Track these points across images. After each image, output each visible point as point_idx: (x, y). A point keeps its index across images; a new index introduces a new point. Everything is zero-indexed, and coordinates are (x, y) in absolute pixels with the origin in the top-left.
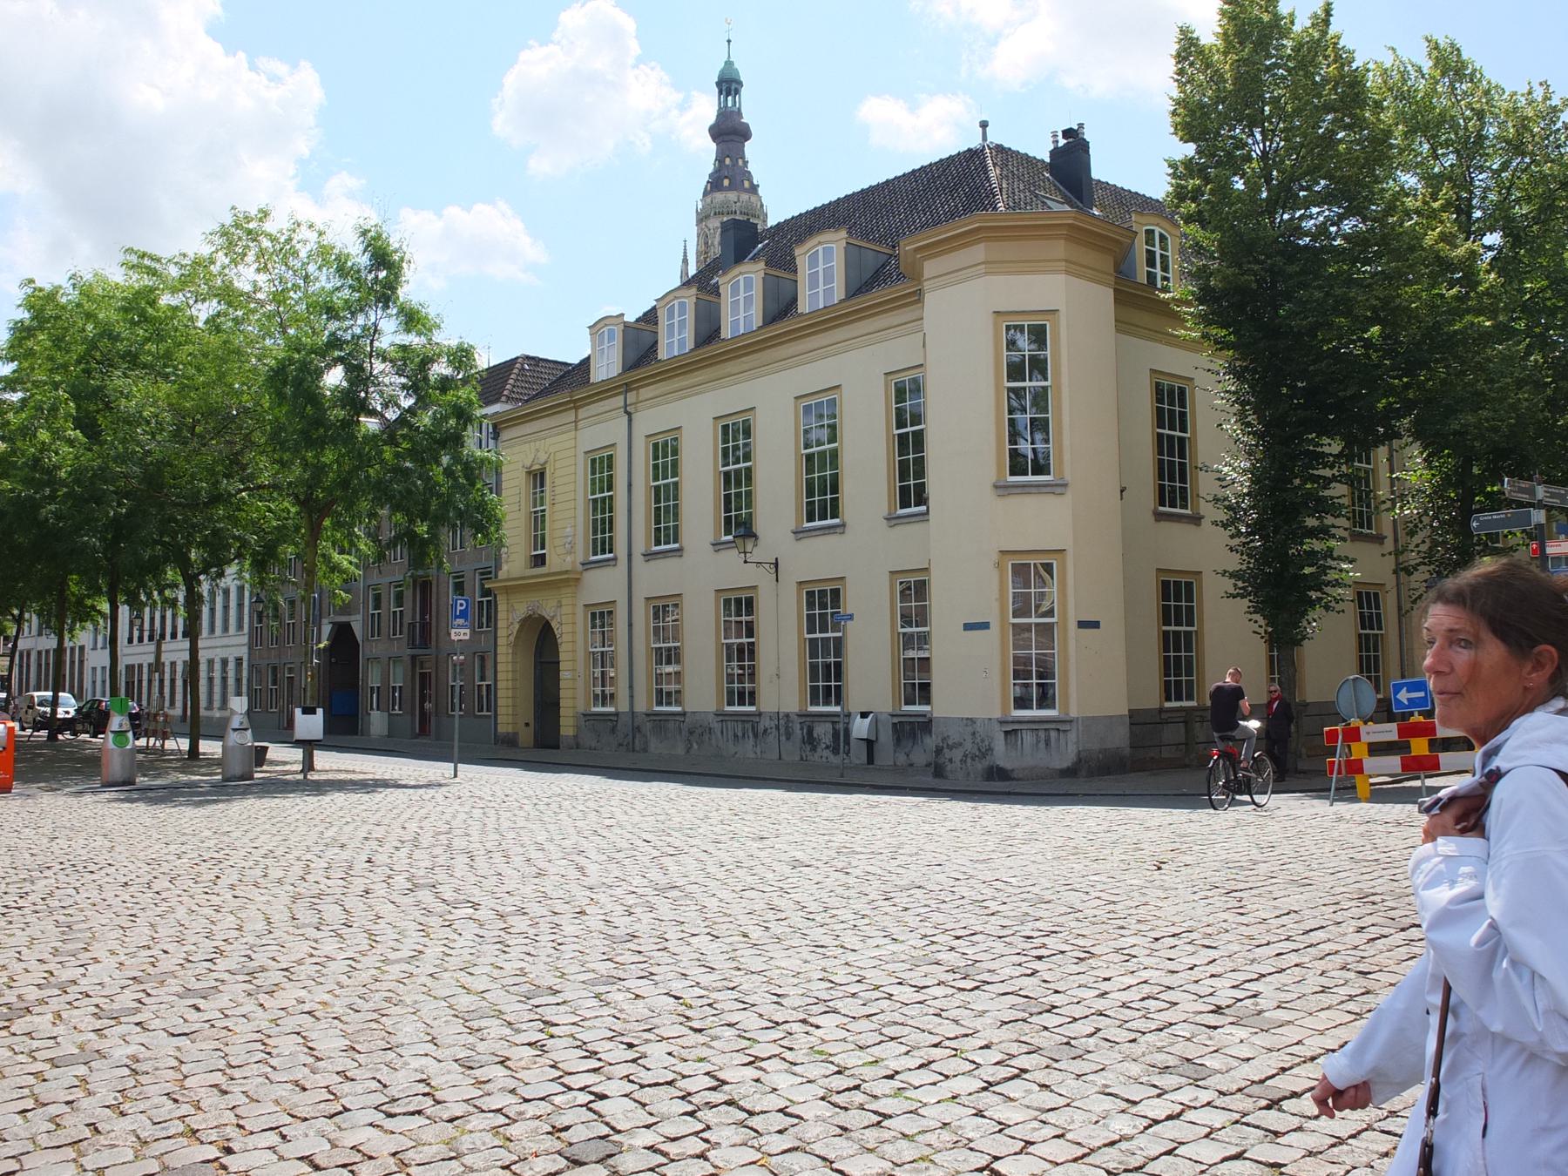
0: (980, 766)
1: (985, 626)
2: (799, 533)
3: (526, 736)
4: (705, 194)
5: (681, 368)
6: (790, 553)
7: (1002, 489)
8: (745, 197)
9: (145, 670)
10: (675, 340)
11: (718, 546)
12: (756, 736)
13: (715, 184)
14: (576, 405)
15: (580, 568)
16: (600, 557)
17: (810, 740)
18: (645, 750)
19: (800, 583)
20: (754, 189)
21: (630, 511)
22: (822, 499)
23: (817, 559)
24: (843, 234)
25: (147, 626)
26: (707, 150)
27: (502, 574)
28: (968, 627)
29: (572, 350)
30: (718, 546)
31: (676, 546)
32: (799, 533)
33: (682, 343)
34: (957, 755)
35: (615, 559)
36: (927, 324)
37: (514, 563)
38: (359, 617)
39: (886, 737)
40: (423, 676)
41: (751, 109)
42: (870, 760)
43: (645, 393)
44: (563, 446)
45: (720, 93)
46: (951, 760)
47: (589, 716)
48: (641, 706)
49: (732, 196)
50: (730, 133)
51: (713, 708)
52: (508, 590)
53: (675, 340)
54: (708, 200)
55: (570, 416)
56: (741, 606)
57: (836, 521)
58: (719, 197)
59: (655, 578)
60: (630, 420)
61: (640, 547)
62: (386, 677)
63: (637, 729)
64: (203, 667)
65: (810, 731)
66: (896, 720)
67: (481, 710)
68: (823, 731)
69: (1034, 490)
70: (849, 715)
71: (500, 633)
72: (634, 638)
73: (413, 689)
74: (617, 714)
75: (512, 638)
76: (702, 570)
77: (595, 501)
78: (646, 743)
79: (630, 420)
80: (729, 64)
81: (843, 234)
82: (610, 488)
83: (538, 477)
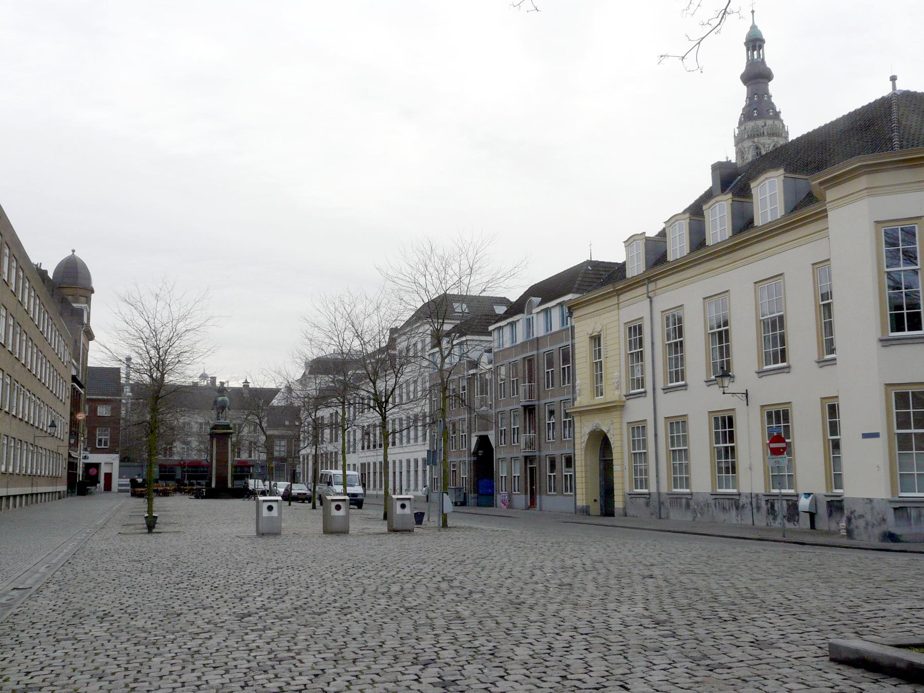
0: (878, 531)
1: (876, 435)
2: (761, 373)
3: (596, 508)
4: (741, 123)
5: (682, 266)
6: (755, 388)
7: (885, 342)
8: (769, 122)
9: (420, 463)
10: (678, 248)
11: (709, 382)
12: (737, 508)
13: (748, 115)
14: (619, 293)
15: (624, 398)
16: (675, 384)
17: (772, 511)
18: (668, 517)
19: (762, 406)
20: (777, 115)
21: (653, 361)
22: (776, 351)
23: (774, 390)
24: (781, 171)
25: (372, 439)
26: (739, 95)
27: (577, 404)
28: (865, 436)
29: (615, 254)
30: (709, 382)
31: (683, 383)
32: (761, 373)
33: (773, 211)
34: (861, 523)
35: (645, 392)
36: (832, 232)
37: (584, 398)
38: (493, 432)
39: (823, 510)
40: (532, 469)
41: (771, 57)
42: (813, 526)
43: (661, 283)
44: (608, 320)
45: (748, 50)
46: (857, 527)
47: (632, 495)
48: (664, 489)
49: (760, 123)
50: (757, 77)
51: (709, 490)
52: (581, 413)
53: (678, 248)
54: (743, 128)
55: (614, 300)
56: (725, 425)
57: (784, 364)
58: (751, 124)
59: (671, 405)
60: (651, 302)
61: (660, 384)
62: (510, 470)
63: (661, 504)
64: (391, 465)
65: (773, 506)
66: (829, 499)
67: (566, 491)
68: (781, 507)
69: (909, 341)
70: (797, 496)
71: (576, 442)
72: (658, 447)
73: (526, 477)
74: (649, 494)
75: (584, 445)
76: (699, 401)
77: (670, 345)
78: (668, 513)
79: (651, 302)
80: (754, 27)
81: (781, 171)
82: (641, 346)
83: (596, 339)
